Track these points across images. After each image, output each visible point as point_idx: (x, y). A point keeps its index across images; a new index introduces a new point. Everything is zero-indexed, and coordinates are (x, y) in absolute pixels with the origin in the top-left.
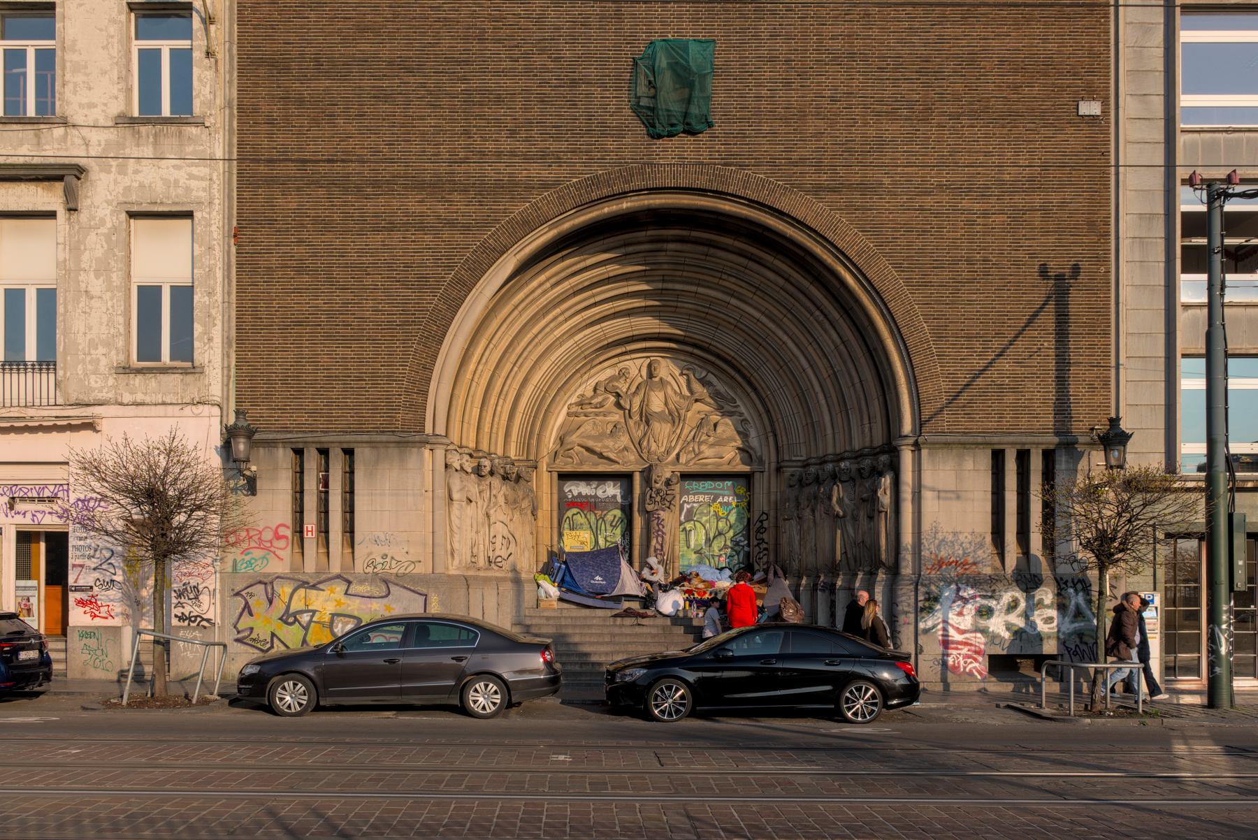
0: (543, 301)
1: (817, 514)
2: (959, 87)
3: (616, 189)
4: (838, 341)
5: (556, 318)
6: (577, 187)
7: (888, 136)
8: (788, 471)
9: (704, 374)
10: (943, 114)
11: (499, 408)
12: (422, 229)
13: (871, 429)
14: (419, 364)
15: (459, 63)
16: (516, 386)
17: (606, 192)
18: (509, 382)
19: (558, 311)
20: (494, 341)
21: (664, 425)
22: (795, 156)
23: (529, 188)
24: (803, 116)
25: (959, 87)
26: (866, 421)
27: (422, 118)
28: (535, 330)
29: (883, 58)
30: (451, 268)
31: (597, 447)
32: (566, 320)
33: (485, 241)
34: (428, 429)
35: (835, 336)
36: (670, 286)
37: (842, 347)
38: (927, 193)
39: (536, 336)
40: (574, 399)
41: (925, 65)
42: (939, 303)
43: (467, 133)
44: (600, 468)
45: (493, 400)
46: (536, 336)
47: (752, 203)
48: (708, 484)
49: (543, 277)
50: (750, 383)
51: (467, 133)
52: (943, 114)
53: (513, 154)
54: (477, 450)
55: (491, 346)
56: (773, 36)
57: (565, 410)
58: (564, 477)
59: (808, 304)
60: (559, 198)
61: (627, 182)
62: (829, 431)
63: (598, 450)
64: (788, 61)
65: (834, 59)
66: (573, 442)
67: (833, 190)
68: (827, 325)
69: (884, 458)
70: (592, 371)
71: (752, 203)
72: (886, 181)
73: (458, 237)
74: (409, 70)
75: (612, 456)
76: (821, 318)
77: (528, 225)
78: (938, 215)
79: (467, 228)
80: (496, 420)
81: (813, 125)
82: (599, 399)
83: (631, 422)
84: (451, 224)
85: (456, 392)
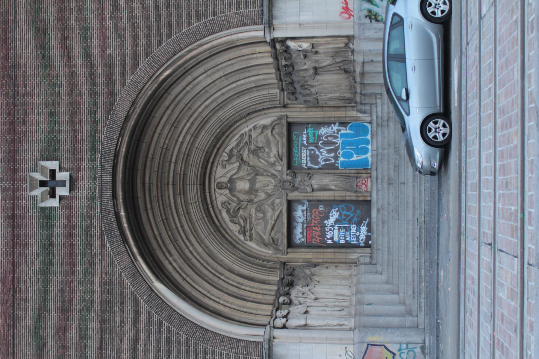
0: (180, 261)
1: (315, 84)
2: (55, 9)
3: (114, 219)
4: (205, 75)
5: (191, 252)
6: (112, 243)
7: (82, 52)
8: (287, 101)
9: (225, 154)
10: (69, 19)
11: (247, 288)
12: (137, 340)
13: (259, 53)
14: (220, 345)
15: (40, 315)
16: (233, 276)
17: (115, 225)
18: (231, 282)
19: (186, 251)
20: (206, 293)
21: (258, 180)
22: (93, 109)
23: (113, 273)
24: (70, 104)
25: (55, 9)
26: (255, 56)
27: (72, 338)
28: (199, 265)
29: (37, 56)
30: (161, 323)
31: (271, 223)
32: (192, 245)
33: (145, 301)
34: (260, 340)
35: (202, 77)
36: (171, 180)
37: (208, 73)
38: (115, 26)
39: (202, 265)
40: (242, 237)
41: (41, 32)
42: (181, 17)
43: (80, 311)
44: (285, 221)
45: (242, 292)
46: (202, 265)
47: (121, 135)
48: (295, 151)
49: (166, 263)
50: (231, 126)
51: (80, 311)
52: (69, 19)
53: (93, 283)
54: (273, 304)
55: (208, 295)
56: (24, 123)
57: (248, 243)
58: (290, 244)
59: (182, 94)
60: (118, 254)
61: (109, 213)
62: (261, 77)
63: (273, 222)
64: (39, 114)
65: (37, 85)
66: (269, 239)
67: (114, 84)
68: (195, 82)
69: (278, 46)
70: (224, 226)
71: (121, 135)
72: (108, 52)
73: (143, 317)
74: (44, 345)
75: (277, 213)
76: (191, 86)
77: (136, 273)
78: (128, 19)
79: (137, 312)
80: (254, 290)
81: (76, 98)
82: (241, 221)
83: (256, 200)
84: (134, 322)
85: (237, 319)
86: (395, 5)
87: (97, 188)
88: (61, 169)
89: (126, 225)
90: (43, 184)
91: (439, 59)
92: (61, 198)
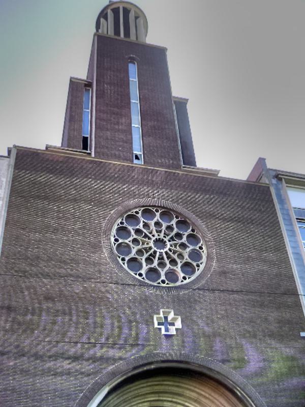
86: (8, 148)
87: (167, 351)
88: (177, 329)
89: (145, 368)
90: (166, 318)
91: (147, 382)
92: (160, 329)
